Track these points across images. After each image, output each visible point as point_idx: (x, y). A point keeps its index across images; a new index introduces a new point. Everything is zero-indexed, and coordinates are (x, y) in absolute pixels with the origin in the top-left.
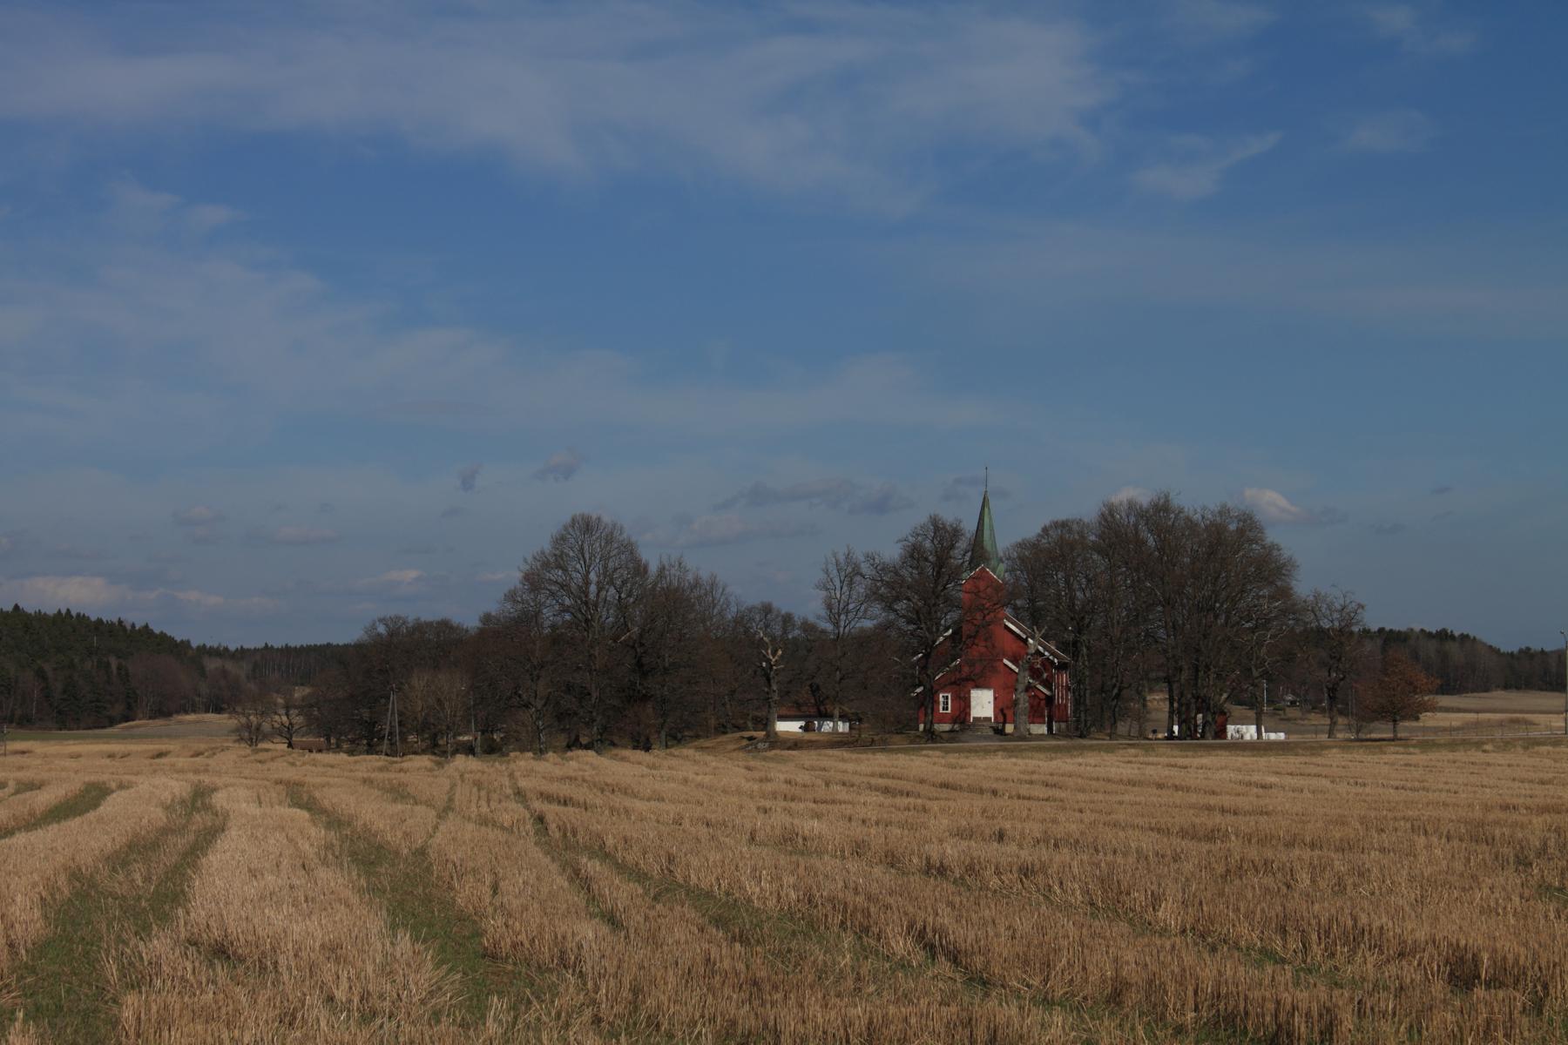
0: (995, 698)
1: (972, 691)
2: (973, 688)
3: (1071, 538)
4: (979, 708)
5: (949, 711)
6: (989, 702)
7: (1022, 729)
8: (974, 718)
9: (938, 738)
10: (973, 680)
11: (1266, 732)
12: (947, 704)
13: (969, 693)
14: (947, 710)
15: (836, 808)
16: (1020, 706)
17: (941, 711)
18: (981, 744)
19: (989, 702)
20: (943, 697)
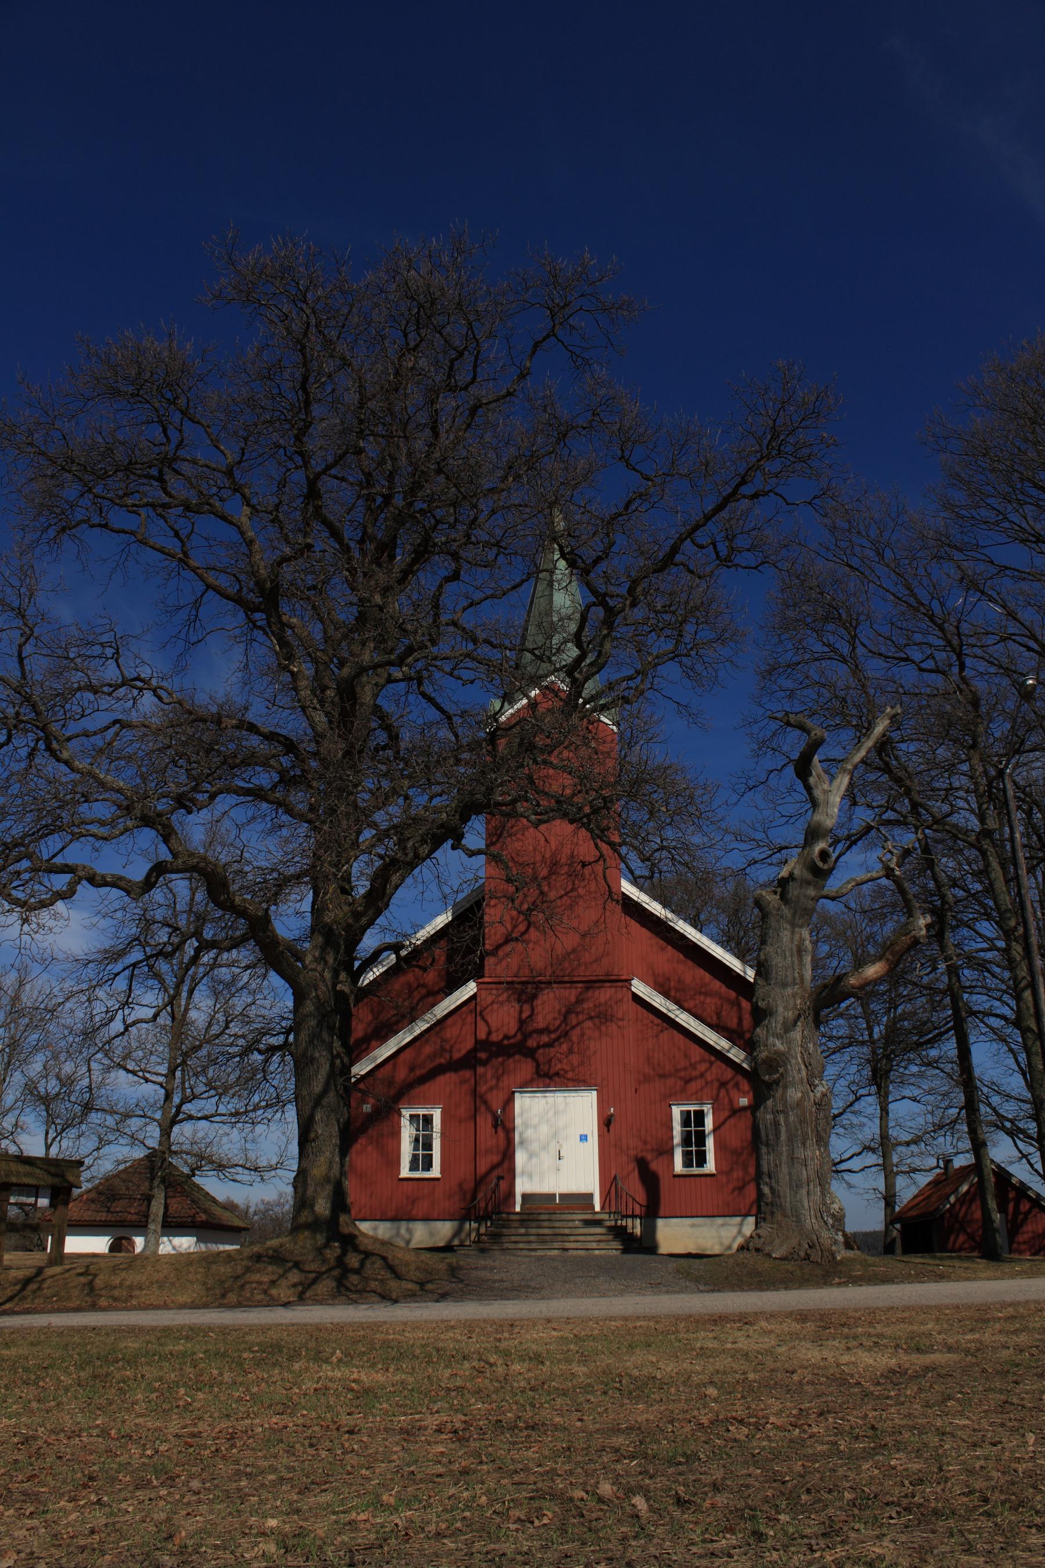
0: (606, 1123)
1: (67, 1238)
2: (526, 1085)
3: (375, 970)
4: (547, 1159)
5: (435, 1172)
6: (584, 1138)
7: (810, 1221)
8: (525, 1197)
9: (374, 1267)
10: (531, 1054)
11: (590, 1196)
12: (428, 1146)
13: (510, 1101)
14: (428, 1165)
15: (71, 1272)
16: (794, 1094)
17: (405, 1172)
18: (222, 1247)
19: (584, 1138)
20: (413, 1118)
